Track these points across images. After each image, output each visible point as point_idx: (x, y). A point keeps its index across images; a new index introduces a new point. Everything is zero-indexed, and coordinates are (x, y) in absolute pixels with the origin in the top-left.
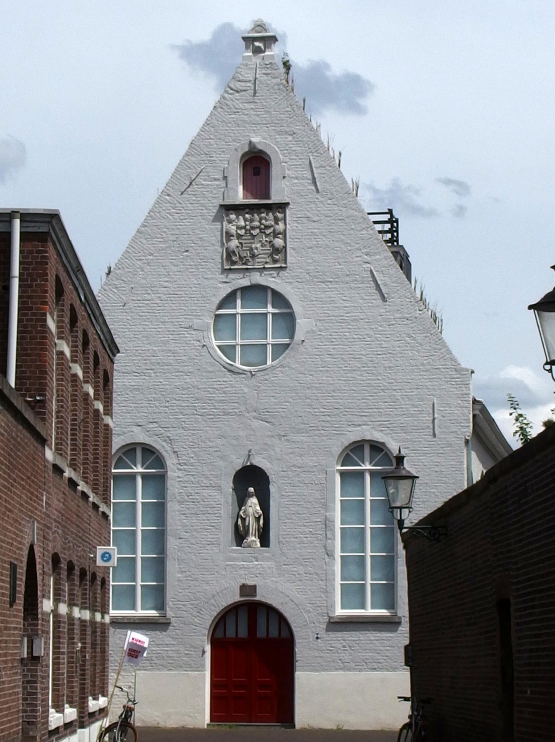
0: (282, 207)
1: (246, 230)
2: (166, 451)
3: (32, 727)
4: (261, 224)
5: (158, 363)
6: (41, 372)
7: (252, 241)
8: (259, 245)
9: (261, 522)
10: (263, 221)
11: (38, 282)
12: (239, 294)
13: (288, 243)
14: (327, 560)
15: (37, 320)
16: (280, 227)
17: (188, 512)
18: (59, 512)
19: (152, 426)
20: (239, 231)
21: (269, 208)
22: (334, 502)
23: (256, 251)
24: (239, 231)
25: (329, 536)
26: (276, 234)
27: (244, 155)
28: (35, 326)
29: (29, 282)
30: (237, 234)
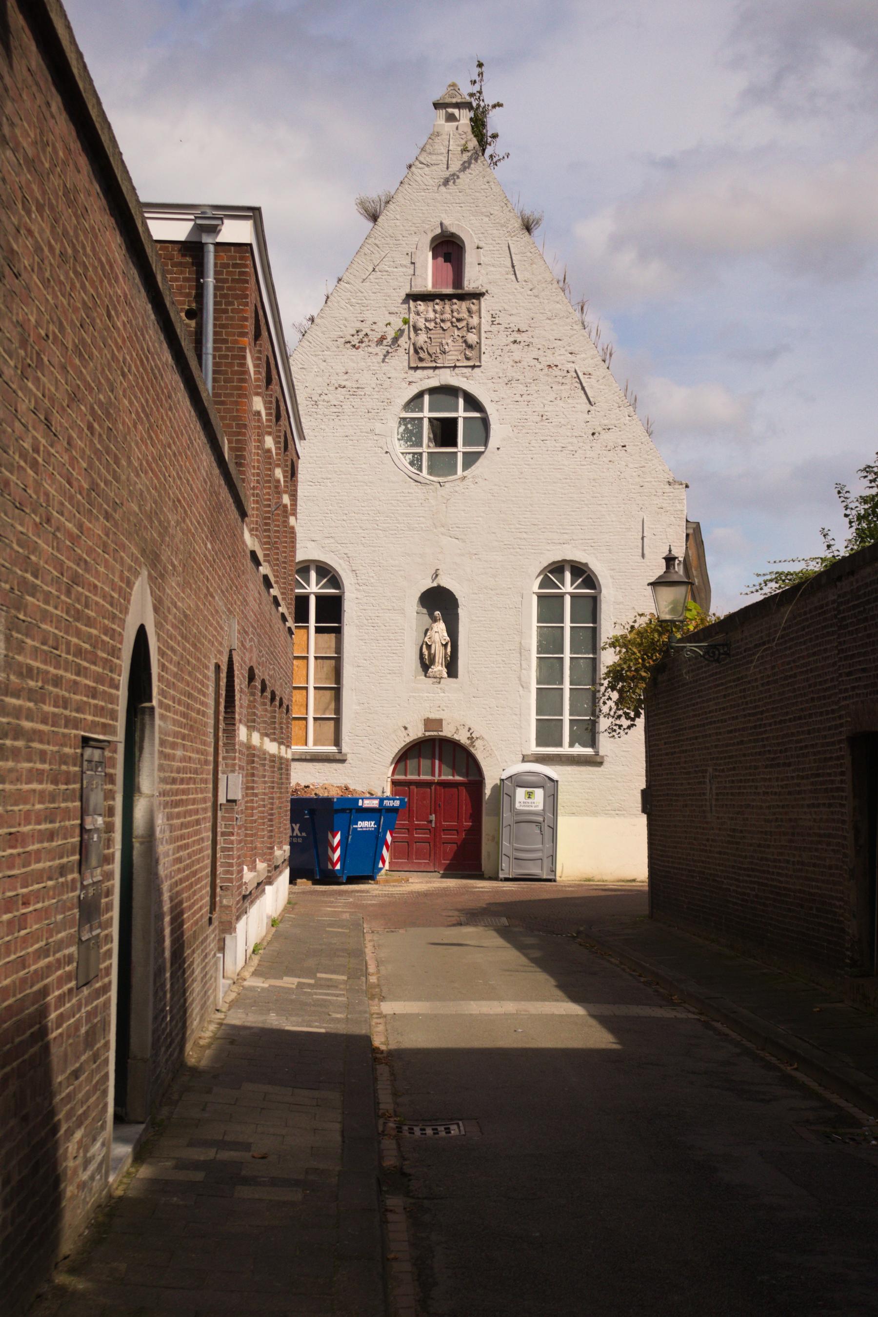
0: (477, 296)
1: (436, 323)
2: (344, 569)
3: (226, 893)
4: (453, 317)
5: (336, 472)
6: (239, 426)
7: (443, 336)
8: (449, 341)
10: (455, 314)
11: (236, 307)
12: (426, 398)
13: (483, 339)
14: (521, 692)
15: (234, 357)
16: (474, 321)
17: (366, 637)
18: (255, 615)
19: (327, 541)
20: (427, 324)
21: (462, 297)
22: (530, 629)
23: (446, 347)
24: (427, 324)
25: (524, 666)
26: (469, 329)
27: (434, 239)
28: (231, 365)
29: (223, 307)
30: (426, 328)
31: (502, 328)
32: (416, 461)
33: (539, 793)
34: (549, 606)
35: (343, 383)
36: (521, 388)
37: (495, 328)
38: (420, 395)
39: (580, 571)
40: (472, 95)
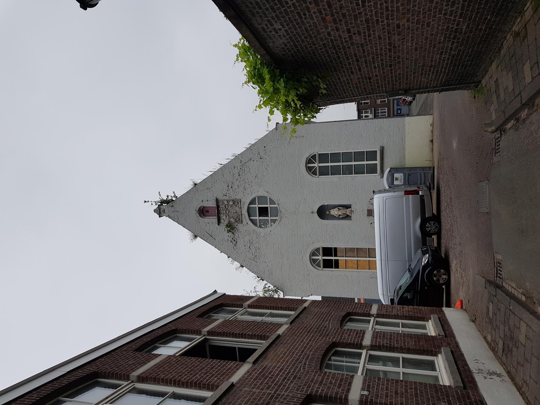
0: (217, 201)
12: (251, 218)
21: (218, 207)
27: (201, 216)
31: (227, 192)
32: (274, 221)
33: (396, 175)
34: (324, 172)
36: (247, 185)
37: (228, 195)
38: (251, 220)
40: (156, 204)
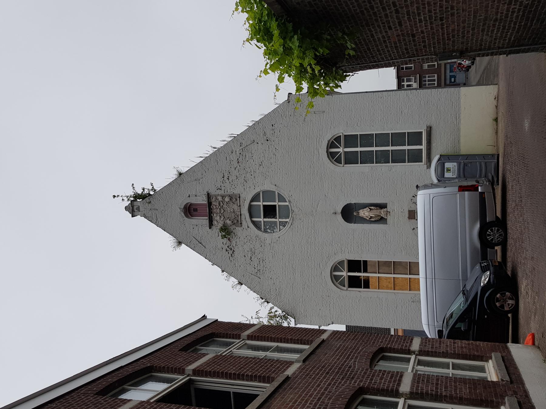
0: (209, 196)
9: (372, 208)
21: (210, 204)
27: (187, 216)
31: (222, 185)
32: (284, 224)
34: (351, 159)
35: (249, 258)
36: (248, 175)
37: (223, 188)
38: (254, 223)
39: (331, 145)
